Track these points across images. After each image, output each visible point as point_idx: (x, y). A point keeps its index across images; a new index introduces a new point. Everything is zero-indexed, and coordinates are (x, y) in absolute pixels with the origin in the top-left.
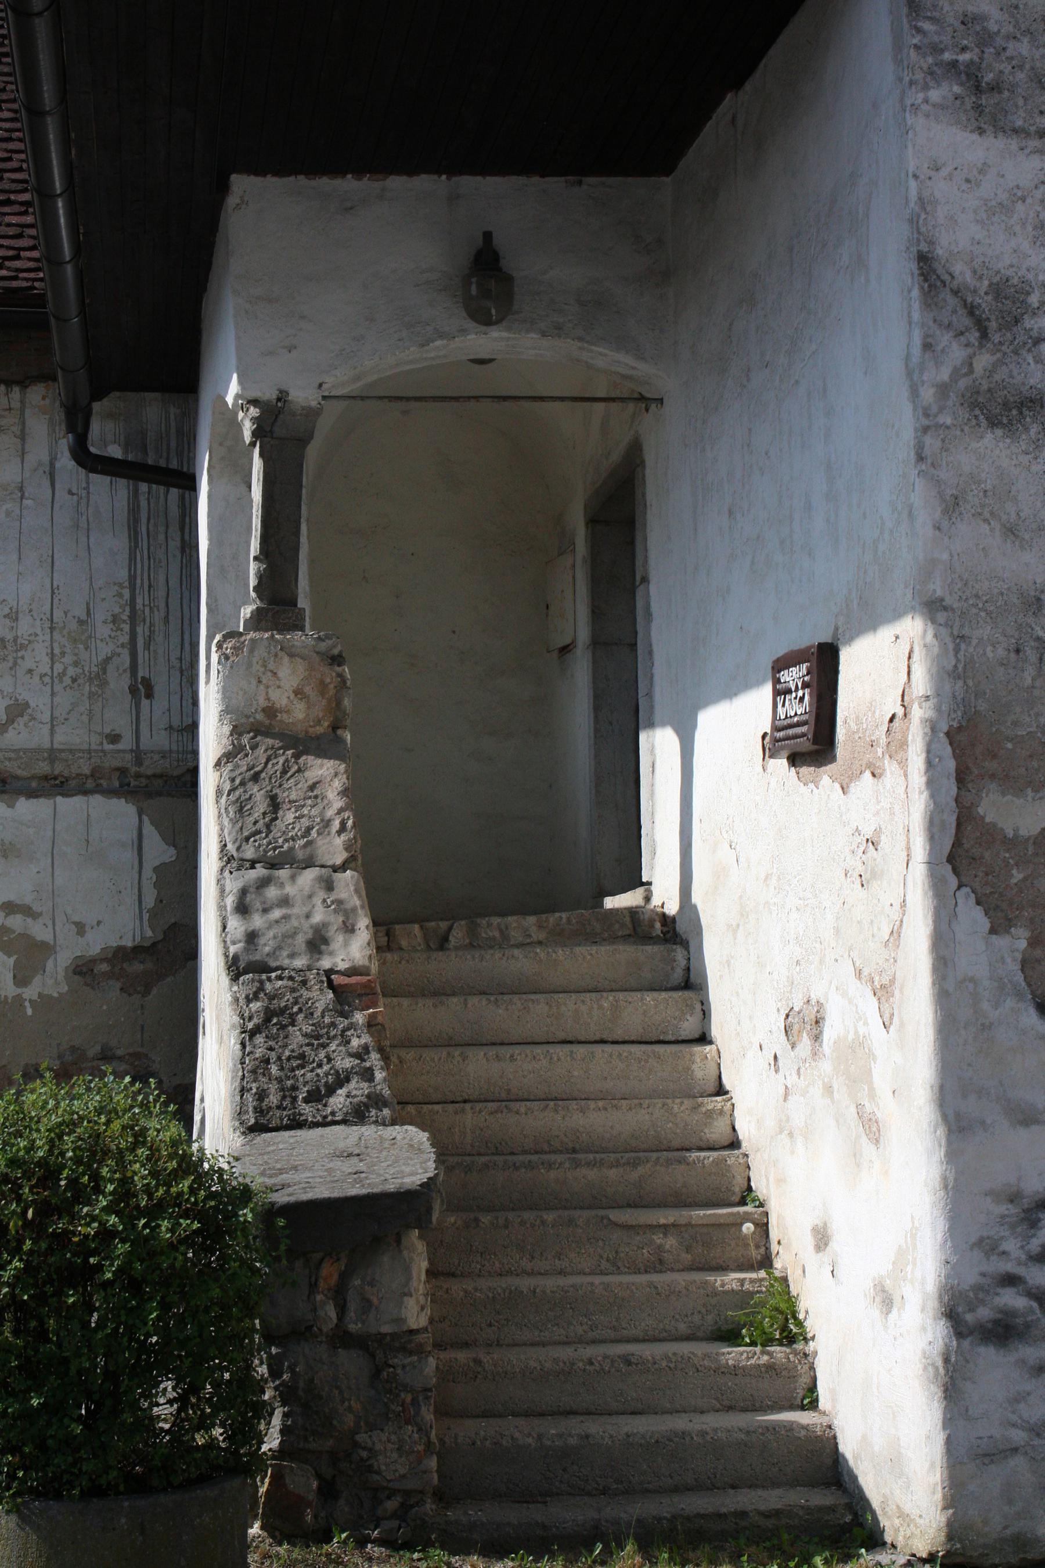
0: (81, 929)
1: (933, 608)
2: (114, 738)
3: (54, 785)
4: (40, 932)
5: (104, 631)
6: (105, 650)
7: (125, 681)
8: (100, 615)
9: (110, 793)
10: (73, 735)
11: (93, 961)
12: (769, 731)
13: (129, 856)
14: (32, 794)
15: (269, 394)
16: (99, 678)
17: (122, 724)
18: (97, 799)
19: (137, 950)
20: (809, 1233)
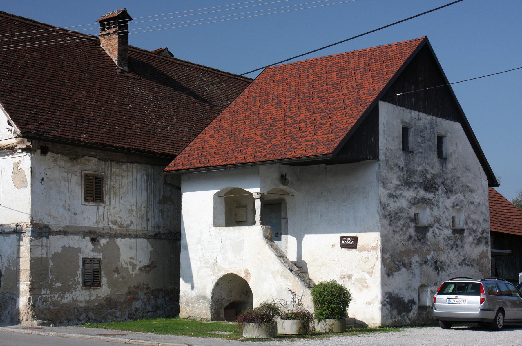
0: (140, 262)
1: (380, 232)
2: (144, 228)
3: (136, 236)
4: (135, 262)
5: (143, 209)
6: (143, 213)
7: (146, 219)
8: (143, 206)
9: (144, 238)
10: (139, 228)
11: (142, 268)
12: (336, 238)
13: (146, 249)
14: (133, 238)
15: (262, 193)
16: (142, 218)
17: (145, 226)
18: (142, 239)
19: (148, 266)
20: (350, 291)
